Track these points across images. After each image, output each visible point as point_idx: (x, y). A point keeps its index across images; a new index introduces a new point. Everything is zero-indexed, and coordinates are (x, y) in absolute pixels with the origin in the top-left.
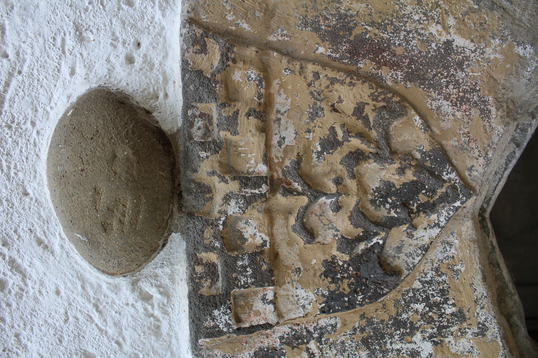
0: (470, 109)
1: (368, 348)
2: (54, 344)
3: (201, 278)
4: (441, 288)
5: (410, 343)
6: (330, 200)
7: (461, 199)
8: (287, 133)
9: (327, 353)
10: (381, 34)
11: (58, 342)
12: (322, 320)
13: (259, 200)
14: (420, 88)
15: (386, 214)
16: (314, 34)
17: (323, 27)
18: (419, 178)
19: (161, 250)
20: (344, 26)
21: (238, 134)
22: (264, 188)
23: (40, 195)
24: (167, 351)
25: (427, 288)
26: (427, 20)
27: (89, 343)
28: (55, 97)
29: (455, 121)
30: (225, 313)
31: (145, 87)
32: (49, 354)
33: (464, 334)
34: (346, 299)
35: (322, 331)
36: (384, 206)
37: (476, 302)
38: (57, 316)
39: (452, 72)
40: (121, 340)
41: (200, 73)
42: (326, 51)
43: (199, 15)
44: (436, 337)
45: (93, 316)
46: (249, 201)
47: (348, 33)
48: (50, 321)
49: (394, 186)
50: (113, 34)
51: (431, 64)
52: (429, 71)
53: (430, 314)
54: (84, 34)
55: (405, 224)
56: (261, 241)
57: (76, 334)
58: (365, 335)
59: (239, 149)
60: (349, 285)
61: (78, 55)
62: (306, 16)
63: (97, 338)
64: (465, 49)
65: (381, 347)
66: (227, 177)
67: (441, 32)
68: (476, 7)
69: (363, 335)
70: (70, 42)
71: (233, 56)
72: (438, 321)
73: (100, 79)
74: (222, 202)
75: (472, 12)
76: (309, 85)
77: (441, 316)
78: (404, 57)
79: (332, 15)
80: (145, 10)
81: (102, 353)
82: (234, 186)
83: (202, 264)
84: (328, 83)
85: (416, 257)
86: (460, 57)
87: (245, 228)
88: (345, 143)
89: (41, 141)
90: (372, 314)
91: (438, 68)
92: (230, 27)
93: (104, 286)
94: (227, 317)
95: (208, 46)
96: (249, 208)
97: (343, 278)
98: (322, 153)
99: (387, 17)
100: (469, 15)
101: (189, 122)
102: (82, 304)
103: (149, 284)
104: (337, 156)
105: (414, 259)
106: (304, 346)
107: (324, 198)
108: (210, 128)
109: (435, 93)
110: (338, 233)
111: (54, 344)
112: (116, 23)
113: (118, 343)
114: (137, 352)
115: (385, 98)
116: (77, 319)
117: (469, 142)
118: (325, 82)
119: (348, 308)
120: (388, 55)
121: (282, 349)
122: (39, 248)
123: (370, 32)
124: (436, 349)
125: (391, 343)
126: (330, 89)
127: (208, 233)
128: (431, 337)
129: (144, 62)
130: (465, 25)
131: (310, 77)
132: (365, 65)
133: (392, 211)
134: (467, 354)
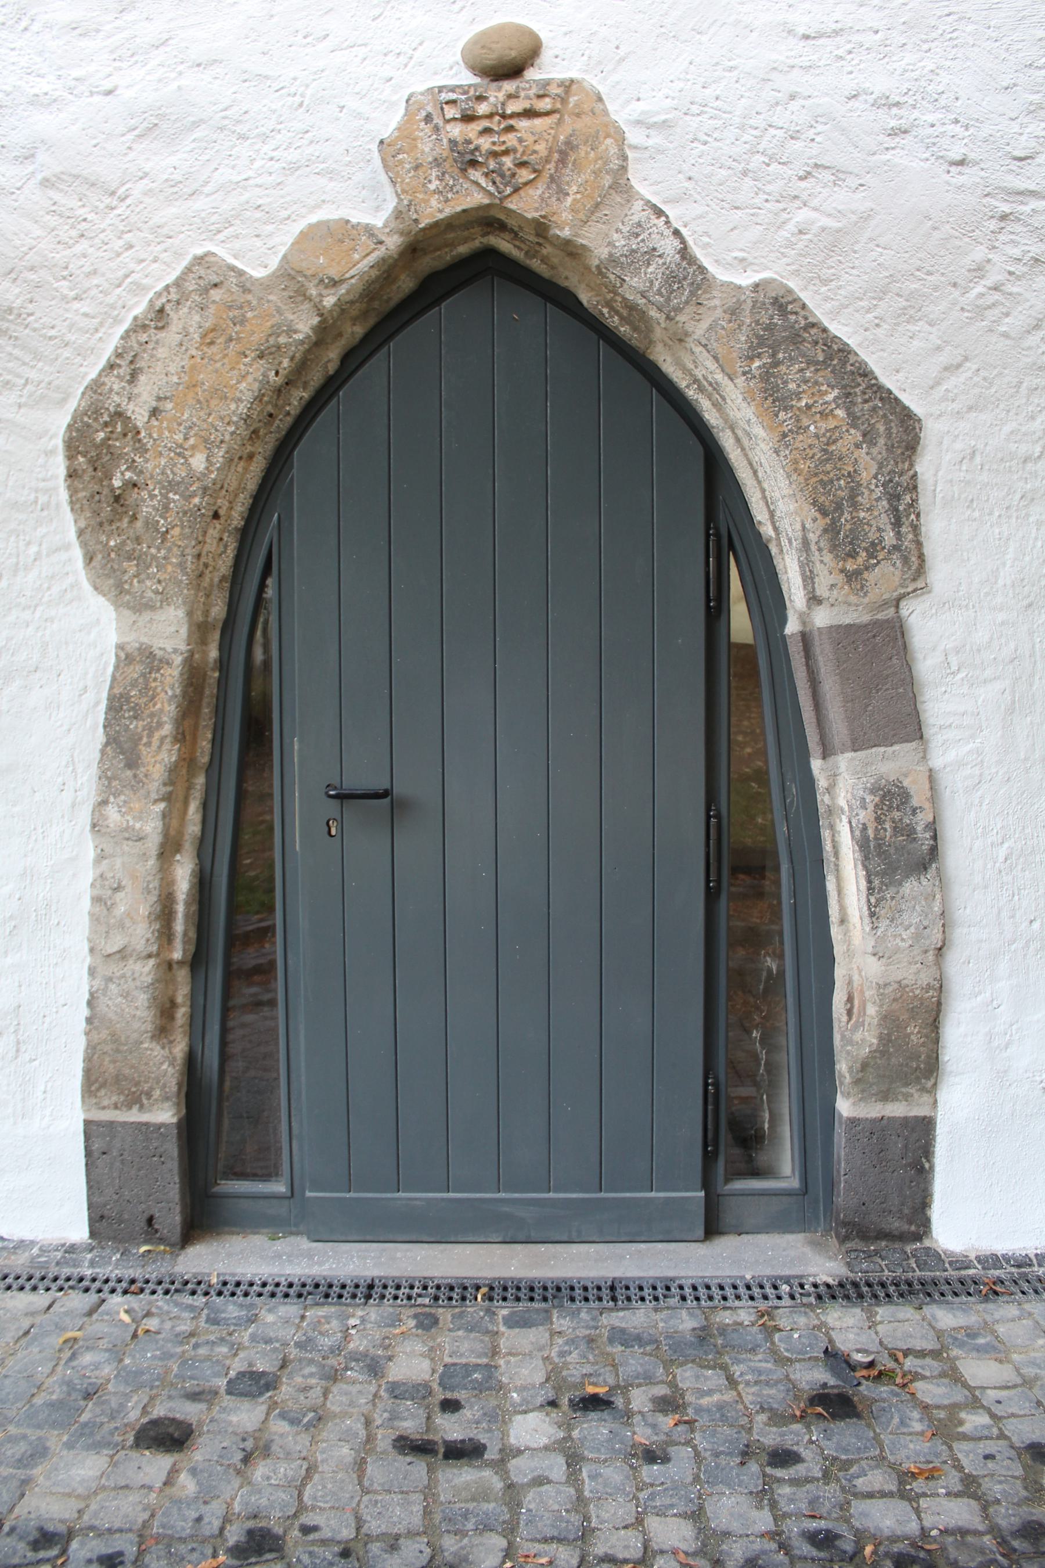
8: (523, 124)
35: (441, 140)
41: (548, 84)
51: (558, 186)
70: (564, 29)
118: (547, 137)
132: (556, 156)
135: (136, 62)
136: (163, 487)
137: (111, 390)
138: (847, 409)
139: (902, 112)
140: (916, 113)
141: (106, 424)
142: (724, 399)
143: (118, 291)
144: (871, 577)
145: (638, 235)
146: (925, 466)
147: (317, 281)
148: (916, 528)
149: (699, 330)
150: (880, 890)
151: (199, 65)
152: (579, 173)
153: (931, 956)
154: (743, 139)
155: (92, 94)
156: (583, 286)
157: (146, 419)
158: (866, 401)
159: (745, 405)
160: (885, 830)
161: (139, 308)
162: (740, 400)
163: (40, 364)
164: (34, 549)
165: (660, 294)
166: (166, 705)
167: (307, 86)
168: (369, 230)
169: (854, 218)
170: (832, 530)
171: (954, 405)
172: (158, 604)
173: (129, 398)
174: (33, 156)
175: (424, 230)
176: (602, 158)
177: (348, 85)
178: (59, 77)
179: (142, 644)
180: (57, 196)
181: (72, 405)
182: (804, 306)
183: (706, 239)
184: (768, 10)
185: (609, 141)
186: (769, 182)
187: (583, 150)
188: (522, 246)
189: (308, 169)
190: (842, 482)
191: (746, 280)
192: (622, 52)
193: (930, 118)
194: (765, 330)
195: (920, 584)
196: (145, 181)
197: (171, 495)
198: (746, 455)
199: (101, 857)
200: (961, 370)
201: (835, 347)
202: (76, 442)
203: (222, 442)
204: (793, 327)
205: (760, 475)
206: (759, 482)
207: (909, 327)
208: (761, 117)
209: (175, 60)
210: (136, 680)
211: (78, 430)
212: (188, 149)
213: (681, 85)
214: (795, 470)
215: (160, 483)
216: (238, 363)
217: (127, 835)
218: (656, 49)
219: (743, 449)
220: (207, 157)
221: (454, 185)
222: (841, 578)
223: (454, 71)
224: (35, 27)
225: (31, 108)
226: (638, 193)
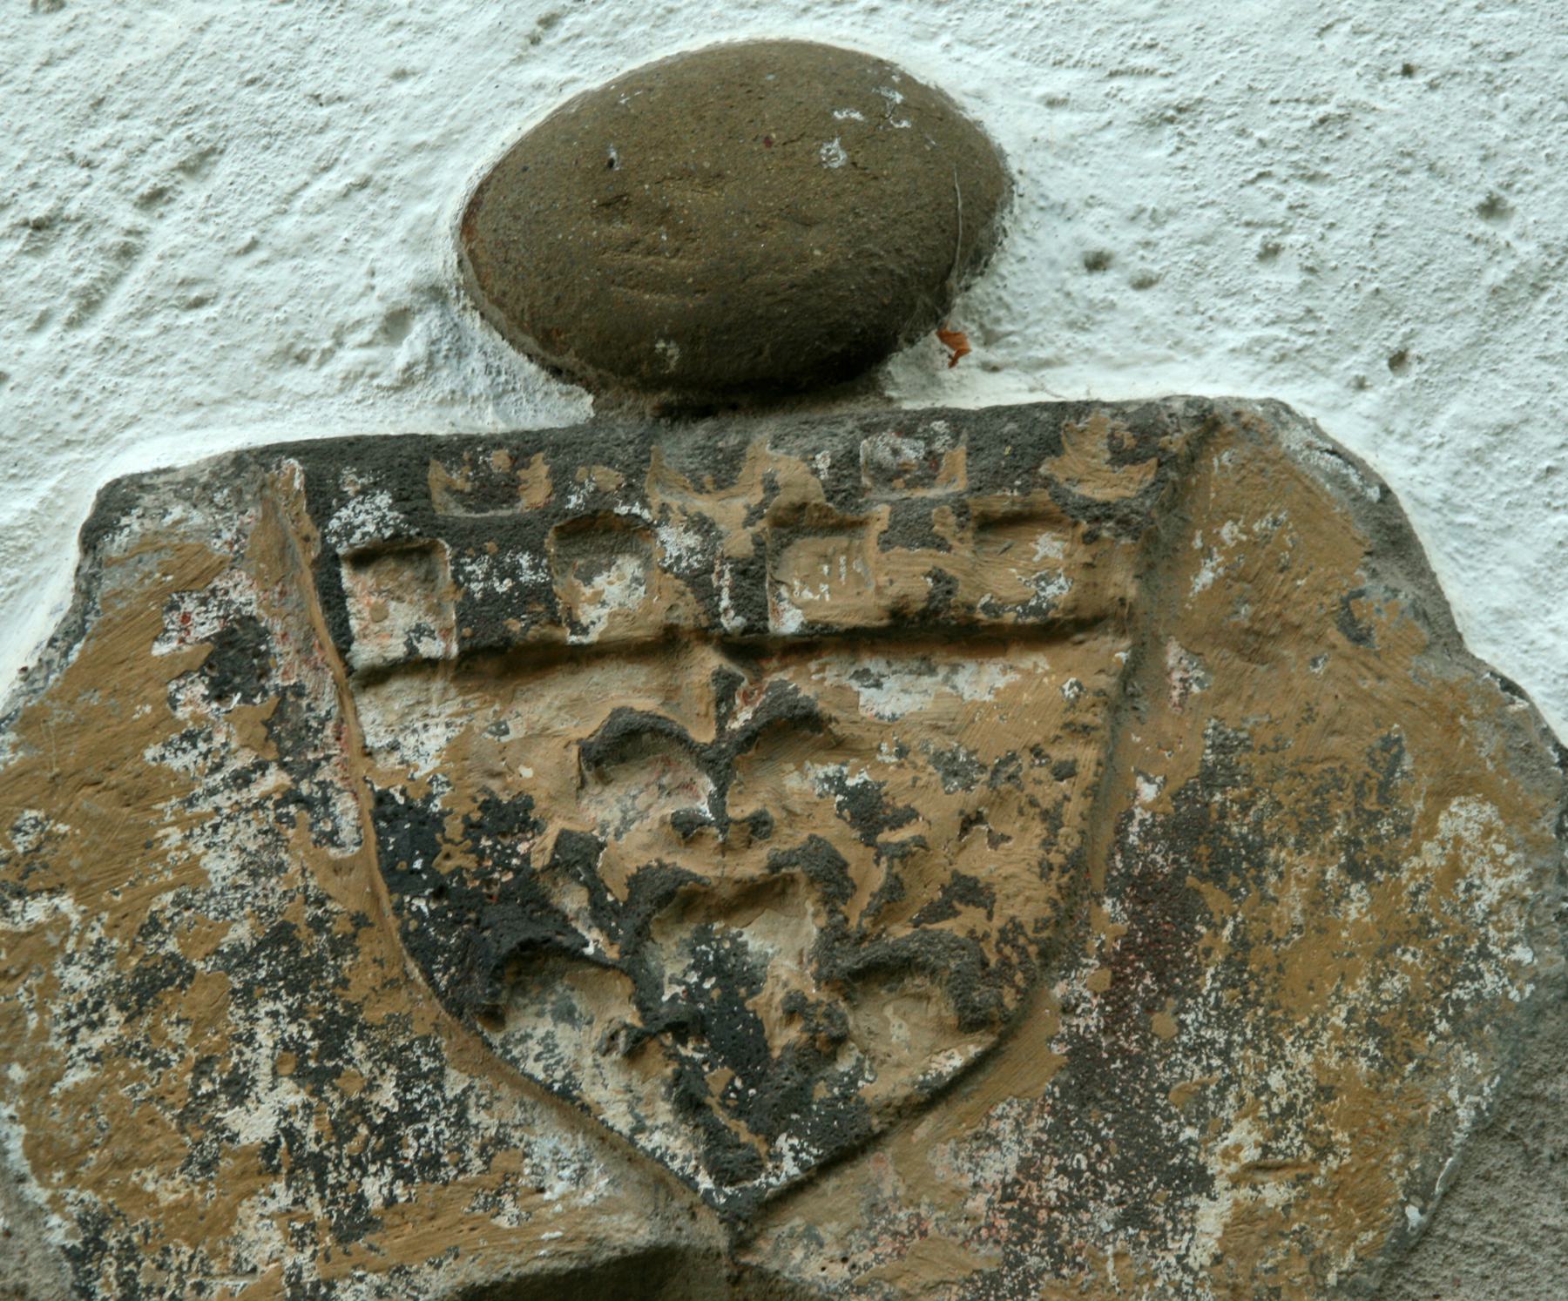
0: (997, 1242)
1: (261, 945)
2: (245, 66)
3: (474, 464)
4: (445, 1159)
5: (275, 1073)
6: (705, 808)
7: (719, 1192)
8: (894, 696)
9: (248, 823)
10: (1211, 970)
11: (248, 77)
12: (351, 803)
13: (701, 609)
14: (1054, 1084)
15: (668, 972)
16: (1196, 771)
17: (1218, 797)
18: (779, 1063)
19: (543, 365)
20: (1226, 859)
21: (883, 550)
22: (732, 622)
23: (687, 20)
24: (228, 388)
25: (444, 1113)
26: (1272, 1117)
27: (248, 163)
28: (980, 57)
29: (957, 1192)
30: (382, 523)
31: (1017, 308)
32: (210, 50)
33: (298, 1239)
34: (418, 865)
35: (318, 805)
36: (694, 967)
37: (399, 1270)
38: (328, 74)
39: (1110, 1189)
40: (260, 255)
41: (1052, 446)
42: (1145, 807)
43: (1230, 444)
44: (290, 1151)
45: (332, 175)
46: (699, 582)
47: (1206, 869)
48: (314, 53)
49: (752, 994)
50: (1171, 213)
52: (1109, 1116)
53: (363, 1130)
54: (1169, 130)
55: (643, 1018)
56: (584, 621)
57: (275, 129)
58: (303, 933)
59: (842, 559)
60: (458, 871)
61: (1106, 117)
62: (1249, 748)
63: (267, 187)
64: (1187, 1236)
65: (264, 982)
66: (762, 524)
67: (1236, 1159)
68: (1332, 1278)
69: (302, 927)
70: (1143, 92)
71: (1105, 534)
72: (339, 1157)
73: (1036, 182)
74: (691, 511)
75: (1312, 1264)
76: (1037, 752)
77: (356, 1162)
78: (1143, 1037)
79: (1259, 823)
80: (1250, 299)
81: (220, 201)
83: (514, 468)
84: (1046, 804)
85: (542, 1064)
86: (1161, 1219)
87: (621, 578)
88: (872, 852)
89: (847, 21)
90: (367, 949)
91: (1119, 1143)
92: (1199, 533)
93: (426, 208)
94: (371, 528)
95: (1134, 469)
96: (678, 582)
97: (481, 855)
98: (842, 789)
99: (1269, 990)
100: (1301, 1254)
102: (370, 144)
103: (435, 333)
105: (538, 1058)
106: (271, 755)
107: (712, 788)
108: (899, 483)
109: (1041, 1130)
110: (611, 838)
111: (245, 66)
112: (1204, 221)
113: (253, 246)
114: (223, 302)
115: (1011, 967)
116: (321, 131)
117: (895, 1234)
118: (1049, 792)
119: (389, 871)
120: (1147, 989)
121: (265, 693)
122: (534, 20)
123: (1216, 935)
124: (253, 1154)
125: (274, 1014)
126: (1027, 809)
127: (607, 477)
128: (291, 1134)
129: (1091, 304)
130: (1266, 1239)
131: (1058, 754)
133: (679, 989)
134: (232, 1255)
176: (1421, 931)
185: (1465, 817)
187: (1294, 875)
221: (410, 1115)
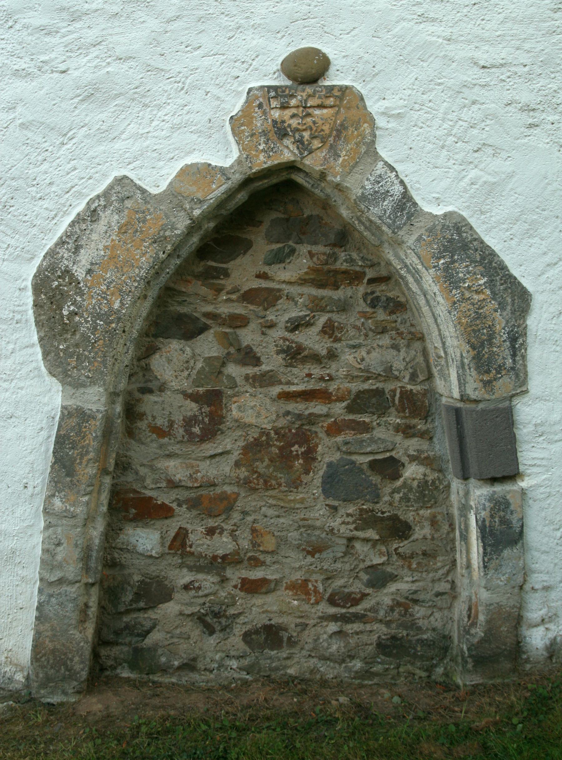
8: (317, 112)
35: (267, 120)
41: (333, 90)
46: (301, 101)
70: (343, 54)
82: (305, 98)
101: (320, 87)
104: (311, 124)
127: (293, 91)
135: (81, 54)
136: (94, 317)
137: (63, 257)
138: (491, 289)
139: (536, 114)
140: (544, 115)
141: (59, 277)
142: (421, 278)
143: (67, 196)
144: (498, 384)
145: (379, 182)
146: (532, 321)
147: (190, 200)
148: (524, 357)
149: (411, 240)
150: (491, 554)
151: (121, 59)
152: (347, 144)
153: (516, 590)
154: (443, 127)
155: (52, 72)
156: (344, 206)
157: (84, 276)
158: (502, 284)
159: (433, 284)
160: (495, 522)
161: (80, 207)
162: (431, 282)
163: (17, 236)
164: (11, 346)
165: (390, 219)
166: (91, 442)
167: (187, 78)
168: (222, 170)
169: (503, 176)
170: (477, 358)
171: (551, 286)
172: (88, 384)
173: (74, 263)
174: (14, 108)
175: (255, 173)
177: (212, 79)
178: (32, 60)
179: (78, 406)
180: (30, 134)
181: (37, 262)
182: (471, 228)
183: (418, 186)
184: (464, 49)
185: (366, 125)
186: (456, 153)
188: (310, 181)
189: (186, 129)
190: (485, 331)
191: (438, 211)
192: (376, 70)
193: (551, 118)
194: (448, 242)
195: (524, 389)
196: (85, 129)
197: (98, 321)
198: (431, 310)
199: (48, 527)
200: (556, 266)
201: (487, 252)
202: (41, 284)
203: (130, 292)
204: (464, 241)
205: (439, 321)
206: (438, 326)
207: (529, 240)
208: (455, 114)
209: (106, 55)
210: (74, 427)
211: (41, 280)
212: (112, 110)
213: (410, 92)
214: (459, 323)
215: (91, 314)
216: (141, 246)
217: (65, 514)
218: (396, 69)
219: (430, 307)
220: (124, 117)
222: (481, 384)
223: (275, 76)
224: (17, 27)
225: (14, 78)
226: (381, 157)
